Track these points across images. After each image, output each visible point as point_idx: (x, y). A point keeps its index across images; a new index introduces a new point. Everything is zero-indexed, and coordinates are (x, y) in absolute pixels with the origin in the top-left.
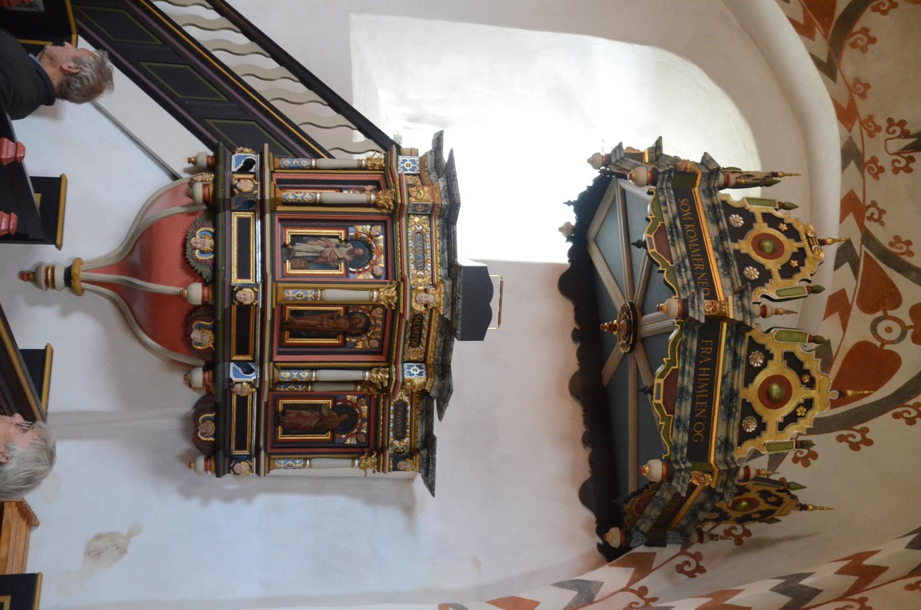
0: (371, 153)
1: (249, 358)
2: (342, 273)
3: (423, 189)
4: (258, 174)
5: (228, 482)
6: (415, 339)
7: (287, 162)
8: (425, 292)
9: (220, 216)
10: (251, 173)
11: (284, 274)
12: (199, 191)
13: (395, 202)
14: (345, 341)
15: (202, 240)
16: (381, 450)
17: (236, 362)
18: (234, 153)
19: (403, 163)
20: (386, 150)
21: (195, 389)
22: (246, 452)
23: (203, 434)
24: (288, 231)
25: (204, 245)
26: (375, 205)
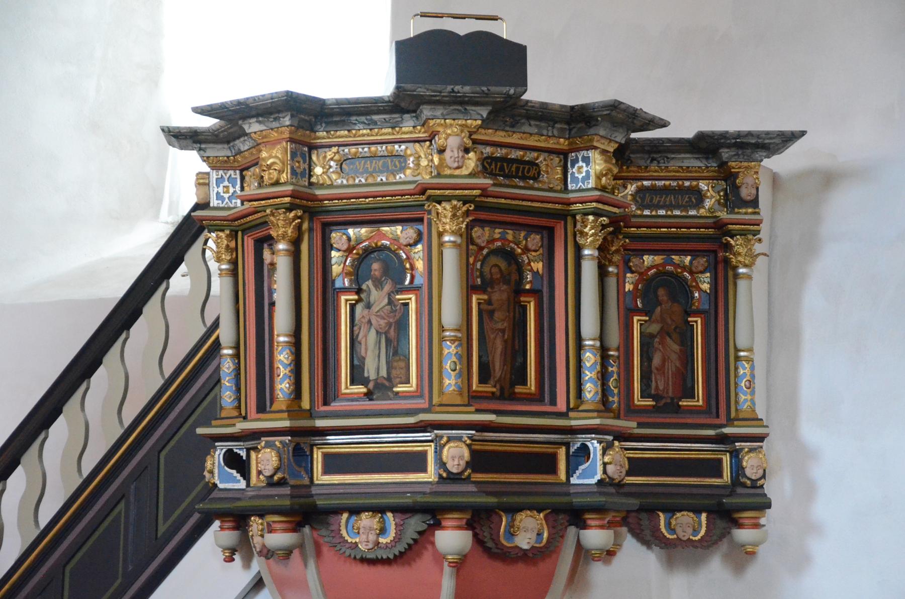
0: (208, 253)
1: (562, 452)
2: (413, 297)
3: (264, 159)
4: (249, 444)
5: (777, 489)
6: (526, 171)
7: (227, 397)
8: (441, 152)
9: (320, 502)
10: (248, 456)
11: (418, 394)
12: (279, 539)
13: (289, 210)
14: (531, 292)
15: (362, 532)
16: (720, 226)
17: (569, 475)
18: (215, 485)
19: (223, 199)
20: (201, 230)
21: (618, 544)
22: (726, 459)
23: (696, 532)
24: (344, 391)
25: (371, 529)
26: (296, 243)
